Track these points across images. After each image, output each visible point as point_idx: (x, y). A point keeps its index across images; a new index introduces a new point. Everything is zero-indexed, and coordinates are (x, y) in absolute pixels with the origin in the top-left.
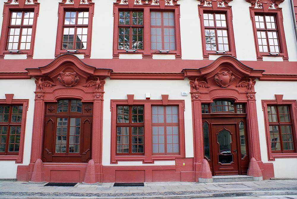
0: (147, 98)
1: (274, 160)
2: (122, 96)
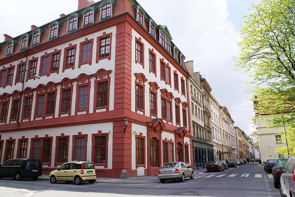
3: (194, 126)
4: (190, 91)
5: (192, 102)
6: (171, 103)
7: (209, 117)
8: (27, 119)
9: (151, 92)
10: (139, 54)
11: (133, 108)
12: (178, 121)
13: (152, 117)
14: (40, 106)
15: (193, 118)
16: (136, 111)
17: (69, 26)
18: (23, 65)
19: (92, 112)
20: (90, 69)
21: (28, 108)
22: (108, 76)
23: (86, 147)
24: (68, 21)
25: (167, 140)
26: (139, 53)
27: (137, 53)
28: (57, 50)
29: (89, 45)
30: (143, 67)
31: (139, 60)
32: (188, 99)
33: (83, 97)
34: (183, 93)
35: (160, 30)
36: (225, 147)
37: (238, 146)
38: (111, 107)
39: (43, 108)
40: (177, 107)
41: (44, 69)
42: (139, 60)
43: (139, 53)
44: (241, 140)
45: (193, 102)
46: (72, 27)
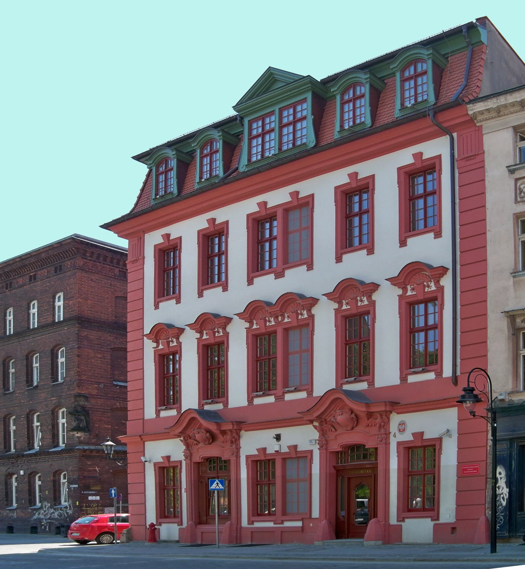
0: (275, 451)
1: (403, 521)
2: (407, 437)
19: (154, 416)
24: (398, 75)
28: (359, 178)
46: (351, 116)
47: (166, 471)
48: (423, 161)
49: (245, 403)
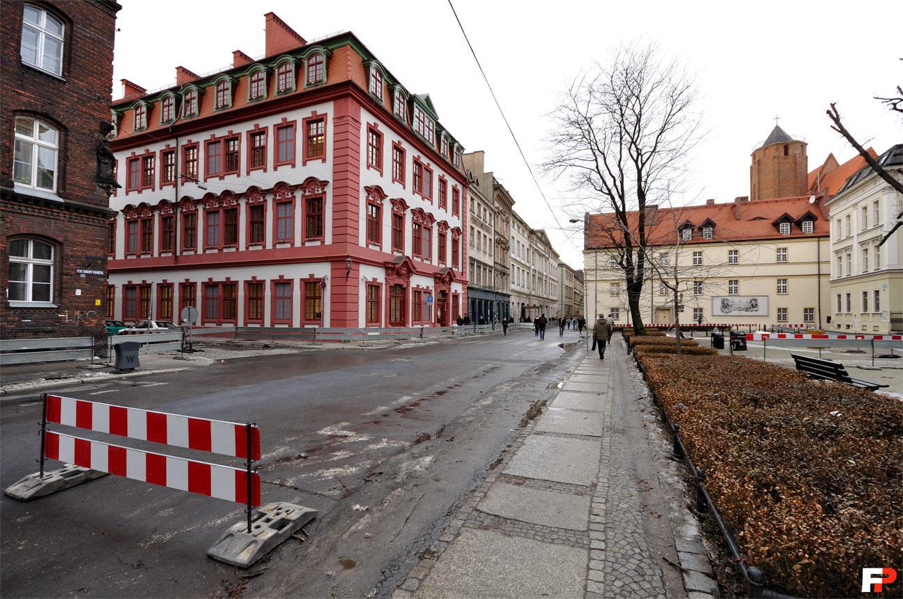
3: (472, 265)
4: (469, 207)
5: (471, 227)
6: (430, 230)
7: (506, 249)
8: (191, 250)
9: (369, 203)
10: (374, 152)
11: (362, 241)
12: (442, 257)
13: (396, 254)
14: (211, 230)
15: (472, 253)
16: (367, 245)
17: (251, 88)
18: (171, 153)
20: (294, 175)
21: (190, 231)
22: (323, 189)
23: (291, 298)
25: (421, 287)
26: (374, 149)
27: (395, 165)
29: (289, 130)
30: (382, 175)
31: (374, 162)
32: (464, 222)
33: (284, 220)
34: (456, 211)
35: (415, 104)
36: (535, 298)
37: (564, 295)
38: (328, 240)
39: (219, 232)
40: (442, 237)
41: (212, 166)
42: (374, 162)
43: (374, 149)
44: (572, 285)
45: (474, 226)
47: (373, 287)
48: (192, 144)
49: (123, 258)
